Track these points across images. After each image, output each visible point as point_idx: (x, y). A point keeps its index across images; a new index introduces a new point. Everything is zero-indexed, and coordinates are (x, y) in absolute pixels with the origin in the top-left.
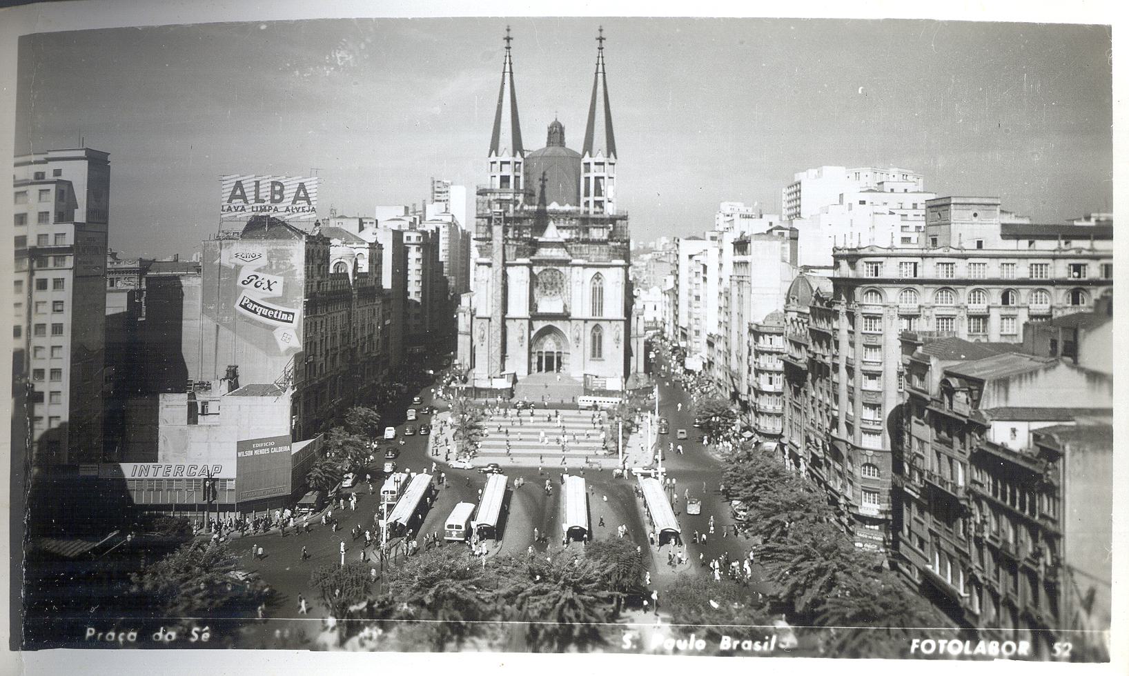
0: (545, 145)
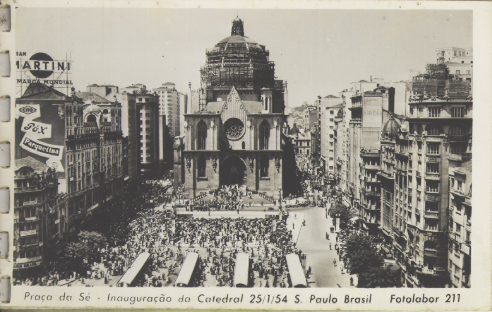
0: (229, 34)
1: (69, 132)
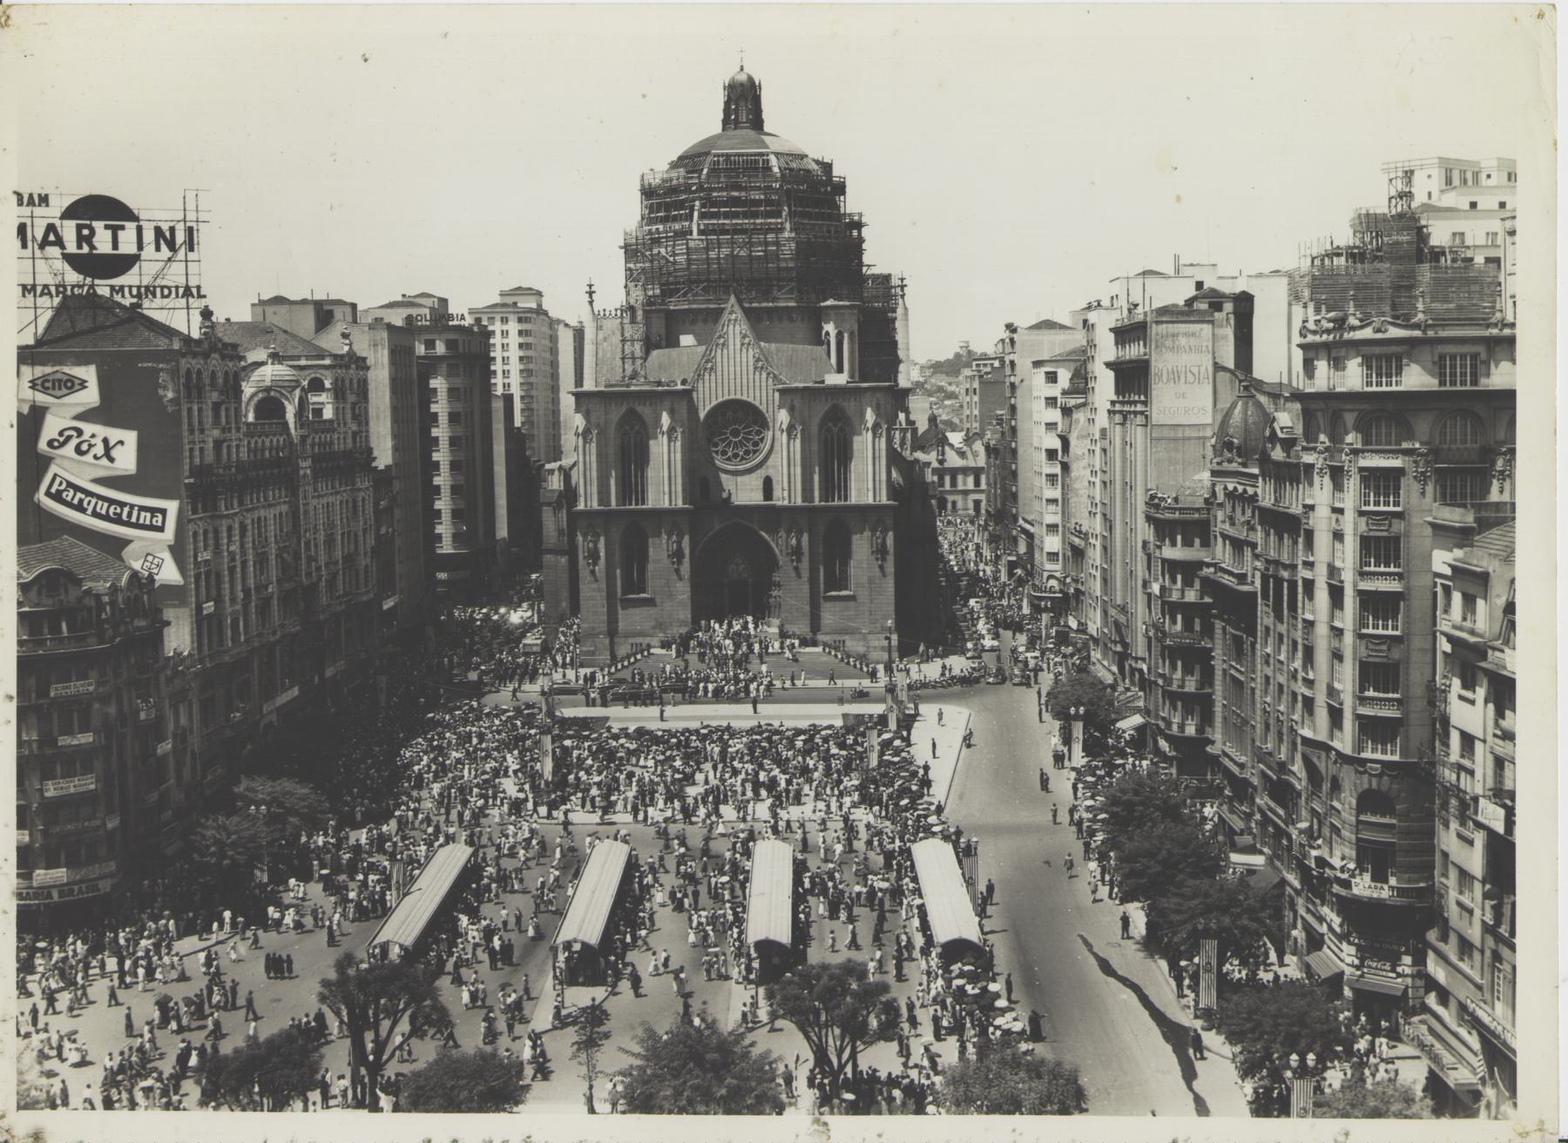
1: (197, 453)
